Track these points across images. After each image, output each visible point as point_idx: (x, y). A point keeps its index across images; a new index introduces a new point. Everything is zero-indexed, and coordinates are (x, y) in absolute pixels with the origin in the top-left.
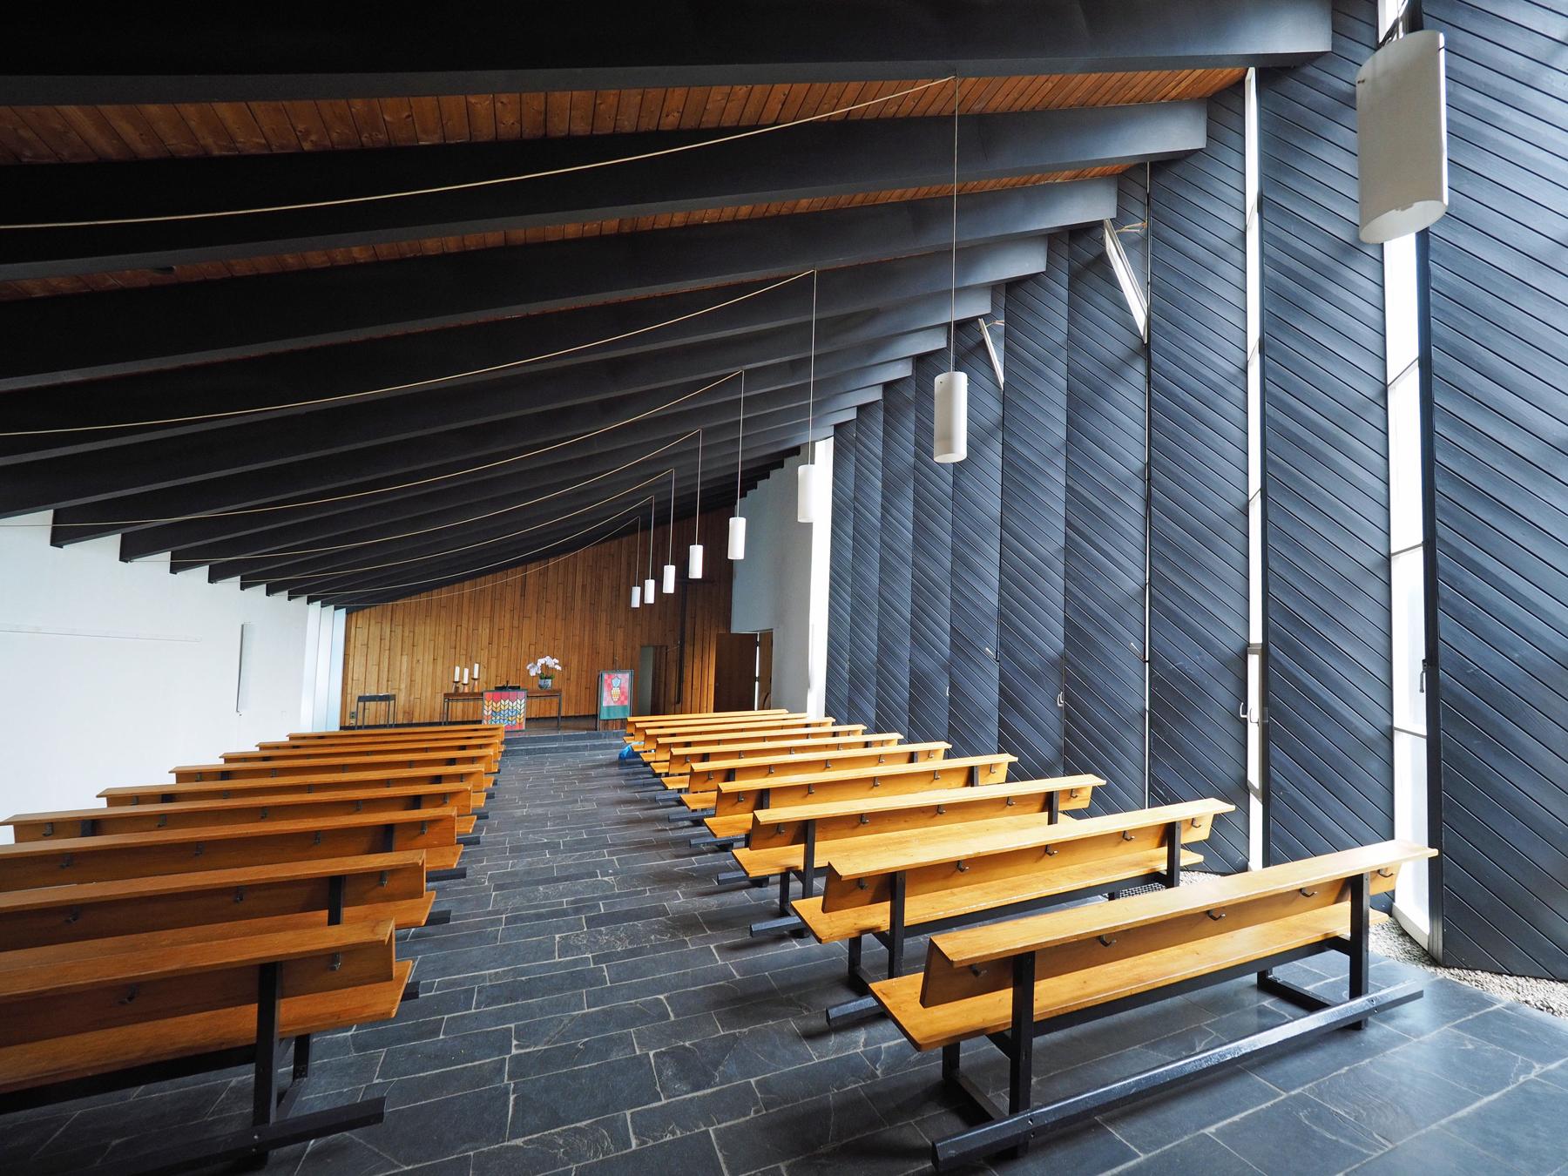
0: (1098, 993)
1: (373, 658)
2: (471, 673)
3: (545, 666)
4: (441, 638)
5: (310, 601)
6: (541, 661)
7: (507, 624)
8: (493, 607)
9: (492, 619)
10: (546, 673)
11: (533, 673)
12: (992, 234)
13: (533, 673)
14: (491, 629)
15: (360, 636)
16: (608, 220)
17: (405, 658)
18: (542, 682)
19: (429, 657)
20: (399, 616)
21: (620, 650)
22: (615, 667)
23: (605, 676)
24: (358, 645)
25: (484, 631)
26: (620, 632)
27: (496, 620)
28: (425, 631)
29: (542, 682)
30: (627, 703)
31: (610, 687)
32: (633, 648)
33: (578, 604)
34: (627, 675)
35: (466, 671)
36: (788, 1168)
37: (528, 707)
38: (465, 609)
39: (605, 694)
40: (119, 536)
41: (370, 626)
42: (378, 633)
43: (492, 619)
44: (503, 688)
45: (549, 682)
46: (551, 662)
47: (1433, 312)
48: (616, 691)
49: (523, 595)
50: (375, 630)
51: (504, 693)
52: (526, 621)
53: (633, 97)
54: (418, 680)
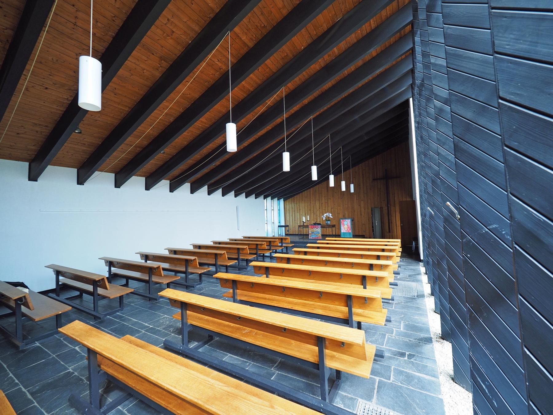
0: (313, 282)
1: (291, 215)
5: (265, 197)
6: (325, 215)
10: (328, 219)
12: (404, 71)
16: (316, 93)
21: (363, 210)
22: (345, 218)
23: (341, 221)
25: (318, 205)
26: (362, 203)
28: (302, 205)
30: (350, 231)
31: (344, 225)
34: (349, 220)
37: (322, 231)
39: (342, 228)
40: (221, 189)
41: (290, 205)
45: (329, 222)
46: (330, 215)
48: (346, 226)
53: (335, 49)
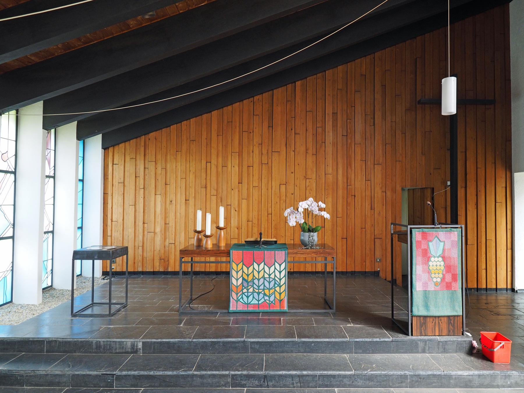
2: (215, 220)
3: (307, 213)
4: (192, 177)
6: (303, 205)
7: (256, 160)
8: (241, 144)
9: (240, 154)
11: (292, 223)
13: (292, 223)
14: (241, 165)
15: (117, 173)
17: (159, 198)
18: (306, 237)
19: (181, 198)
20: (151, 150)
21: (378, 193)
23: (417, 234)
24: (116, 183)
27: (245, 155)
29: (306, 237)
31: (426, 255)
32: (394, 191)
33: (330, 137)
35: (209, 216)
36: (284, 307)
38: (214, 144)
42: (133, 170)
43: (240, 154)
44: (255, 244)
45: (315, 236)
47: (5, 302)
48: (436, 263)
49: (271, 126)
50: (130, 167)
51: (257, 252)
52: (275, 156)
54: (172, 224)
